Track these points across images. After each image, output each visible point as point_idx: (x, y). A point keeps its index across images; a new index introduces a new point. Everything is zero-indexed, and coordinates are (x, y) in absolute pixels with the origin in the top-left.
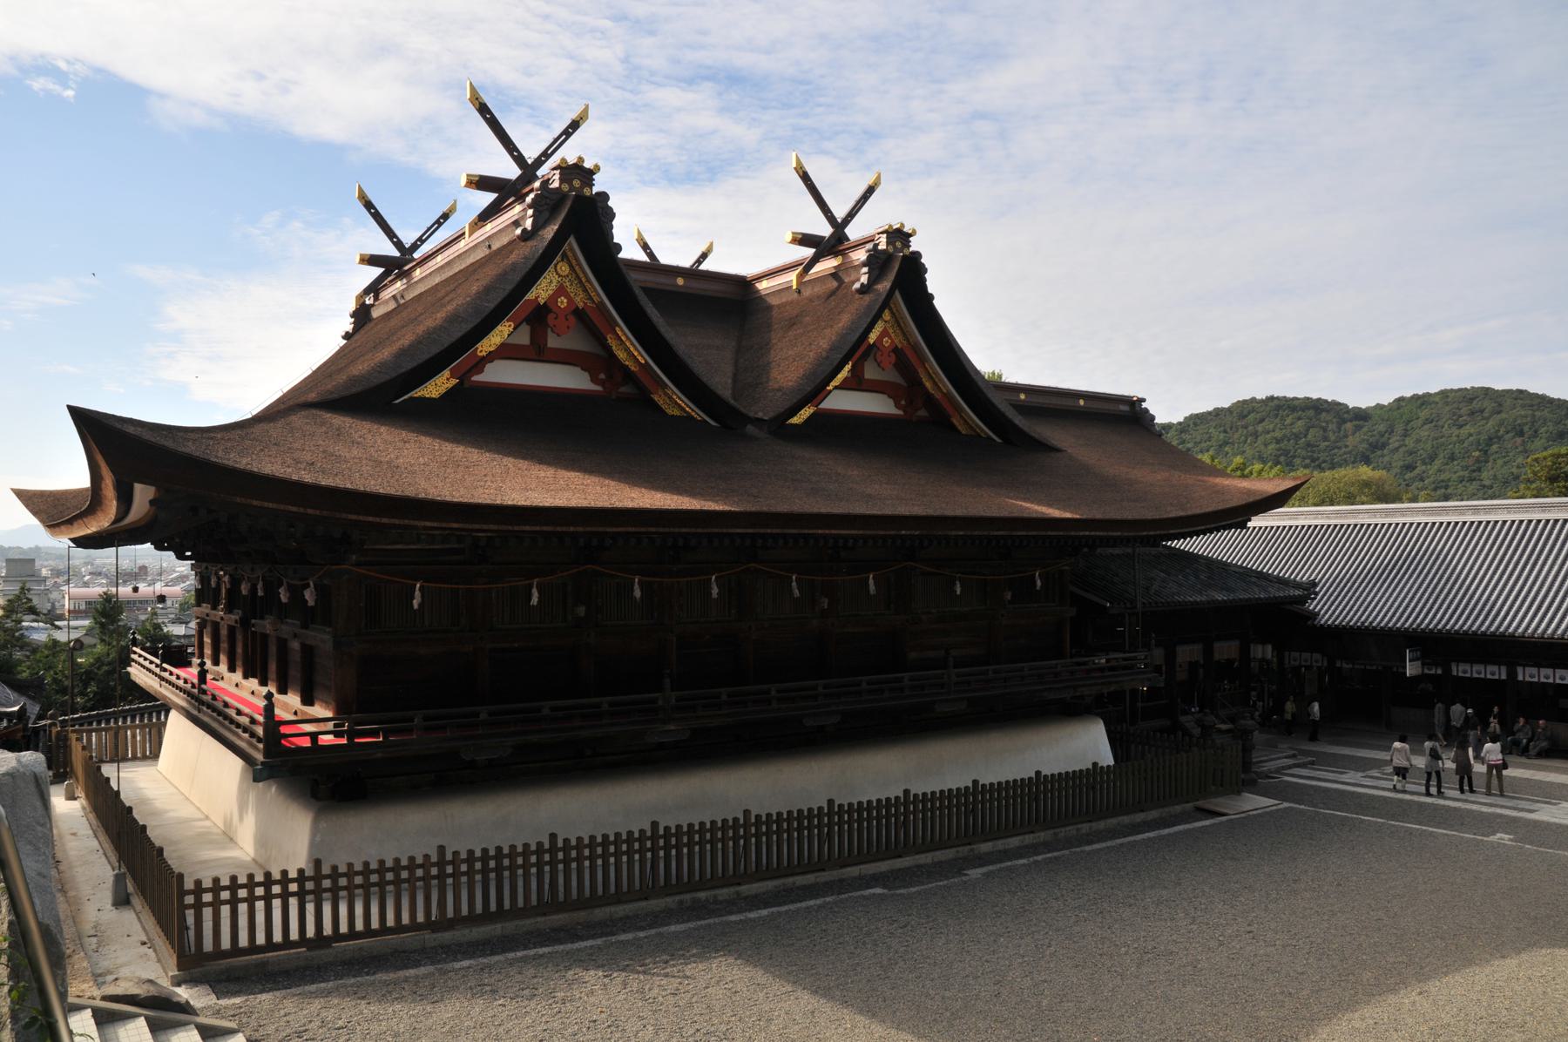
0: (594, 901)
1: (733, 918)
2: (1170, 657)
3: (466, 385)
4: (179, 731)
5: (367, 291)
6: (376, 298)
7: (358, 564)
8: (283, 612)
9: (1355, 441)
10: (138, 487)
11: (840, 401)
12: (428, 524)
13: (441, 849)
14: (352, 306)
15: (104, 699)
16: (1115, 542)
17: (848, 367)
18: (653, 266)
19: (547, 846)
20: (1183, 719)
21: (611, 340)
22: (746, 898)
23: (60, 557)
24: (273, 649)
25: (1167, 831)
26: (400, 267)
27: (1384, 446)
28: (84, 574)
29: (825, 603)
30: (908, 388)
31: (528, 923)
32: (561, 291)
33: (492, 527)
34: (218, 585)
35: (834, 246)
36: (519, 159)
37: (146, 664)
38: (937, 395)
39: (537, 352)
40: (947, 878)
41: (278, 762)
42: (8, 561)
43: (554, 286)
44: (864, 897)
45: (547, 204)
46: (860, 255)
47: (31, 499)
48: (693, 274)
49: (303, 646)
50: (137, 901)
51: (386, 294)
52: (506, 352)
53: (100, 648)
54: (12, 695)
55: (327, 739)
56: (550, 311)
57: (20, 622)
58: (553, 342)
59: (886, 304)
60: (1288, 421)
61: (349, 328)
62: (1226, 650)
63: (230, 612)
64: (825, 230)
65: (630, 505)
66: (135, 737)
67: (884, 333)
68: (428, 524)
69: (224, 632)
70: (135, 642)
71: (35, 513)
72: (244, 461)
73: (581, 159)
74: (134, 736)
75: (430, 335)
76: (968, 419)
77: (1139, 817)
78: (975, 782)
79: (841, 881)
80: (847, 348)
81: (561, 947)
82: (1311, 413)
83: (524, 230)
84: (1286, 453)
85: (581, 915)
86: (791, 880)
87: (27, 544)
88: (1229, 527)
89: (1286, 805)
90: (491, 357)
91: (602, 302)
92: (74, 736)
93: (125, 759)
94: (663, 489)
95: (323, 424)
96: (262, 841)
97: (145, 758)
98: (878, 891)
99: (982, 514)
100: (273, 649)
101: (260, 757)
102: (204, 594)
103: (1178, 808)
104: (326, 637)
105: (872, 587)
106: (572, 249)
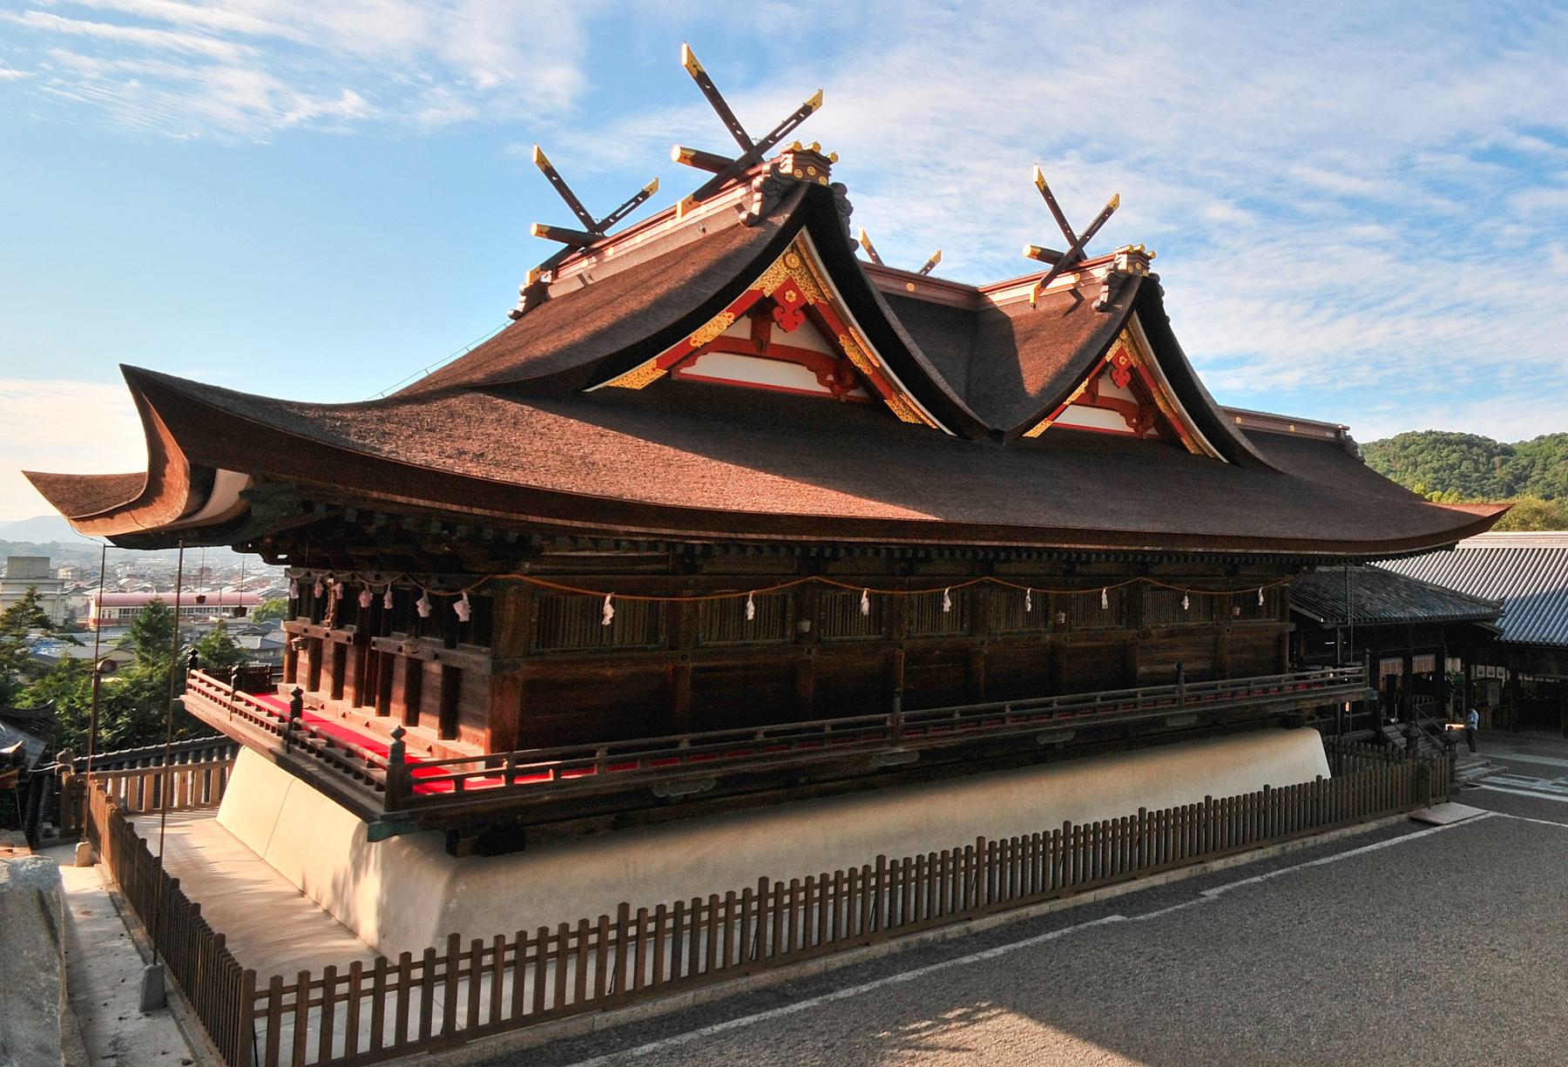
0: (809, 951)
1: (967, 960)
2: (1375, 669)
3: (675, 377)
4: (254, 776)
5: (545, 267)
6: (555, 276)
7: (531, 574)
8: (420, 628)
9: (1502, 473)
10: (223, 475)
11: (1075, 416)
12: (633, 529)
13: (624, 907)
14: (527, 282)
15: (144, 730)
16: (1330, 561)
17: (1085, 383)
18: (879, 269)
19: (755, 893)
20: (1386, 729)
21: (843, 341)
22: (977, 934)
23: (87, 556)
24: (401, 672)
25: (1386, 843)
26: (587, 244)
27: (1527, 478)
28: (107, 576)
29: (1062, 617)
30: (1141, 406)
31: (728, 987)
32: (789, 284)
33: (713, 534)
34: (325, 595)
35: (1071, 264)
36: (744, 140)
37: (211, 691)
38: (1169, 415)
39: (758, 347)
40: (1185, 901)
41: (403, 807)
42: (10, 559)
43: (782, 279)
44: (1104, 926)
45: (778, 190)
46: (1100, 273)
47: (48, 485)
48: (921, 280)
49: (446, 669)
50: (178, 1003)
51: (570, 272)
52: (724, 345)
53: (138, 670)
54: (11, 732)
55: (476, 783)
56: (777, 305)
57: (23, 636)
58: (777, 337)
59: (1123, 325)
60: (1445, 453)
61: (520, 307)
62: (1424, 664)
63: (340, 627)
64: (1064, 247)
65: (871, 515)
66: (184, 779)
67: (1121, 352)
68: (633, 529)
69: (328, 651)
70: (194, 664)
71: (56, 503)
72: (387, 448)
73: (817, 145)
74: (184, 780)
75: (634, 318)
76: (1197, 440)
77: (1359, 829)
78: (1208, 798)
79: (1077, 908)
80: (1085, 365)
81: (769, 1013)
82: (1464, 447)
83: (750, 215)
84: (1442, 482)
85: (792, 972)
86: (1024, 911)
87: (39, 538)
88: (1441, 549)
89: (1491, 814)
90: (706, 349)
91: (835, 300)
92: (93, 785)
93: (168, 809)
94: (870, 496)
95: (494, 409)
96: (388, 917)
97: (198, 806)
98: (1117, 918)
99: (830, 512)
100: (401, 672)
101: (379, 810)
102: (305, 605)
103: (1394, 819)
104: (482, 659)
105: (1105, 602)
106: (803, 241)
